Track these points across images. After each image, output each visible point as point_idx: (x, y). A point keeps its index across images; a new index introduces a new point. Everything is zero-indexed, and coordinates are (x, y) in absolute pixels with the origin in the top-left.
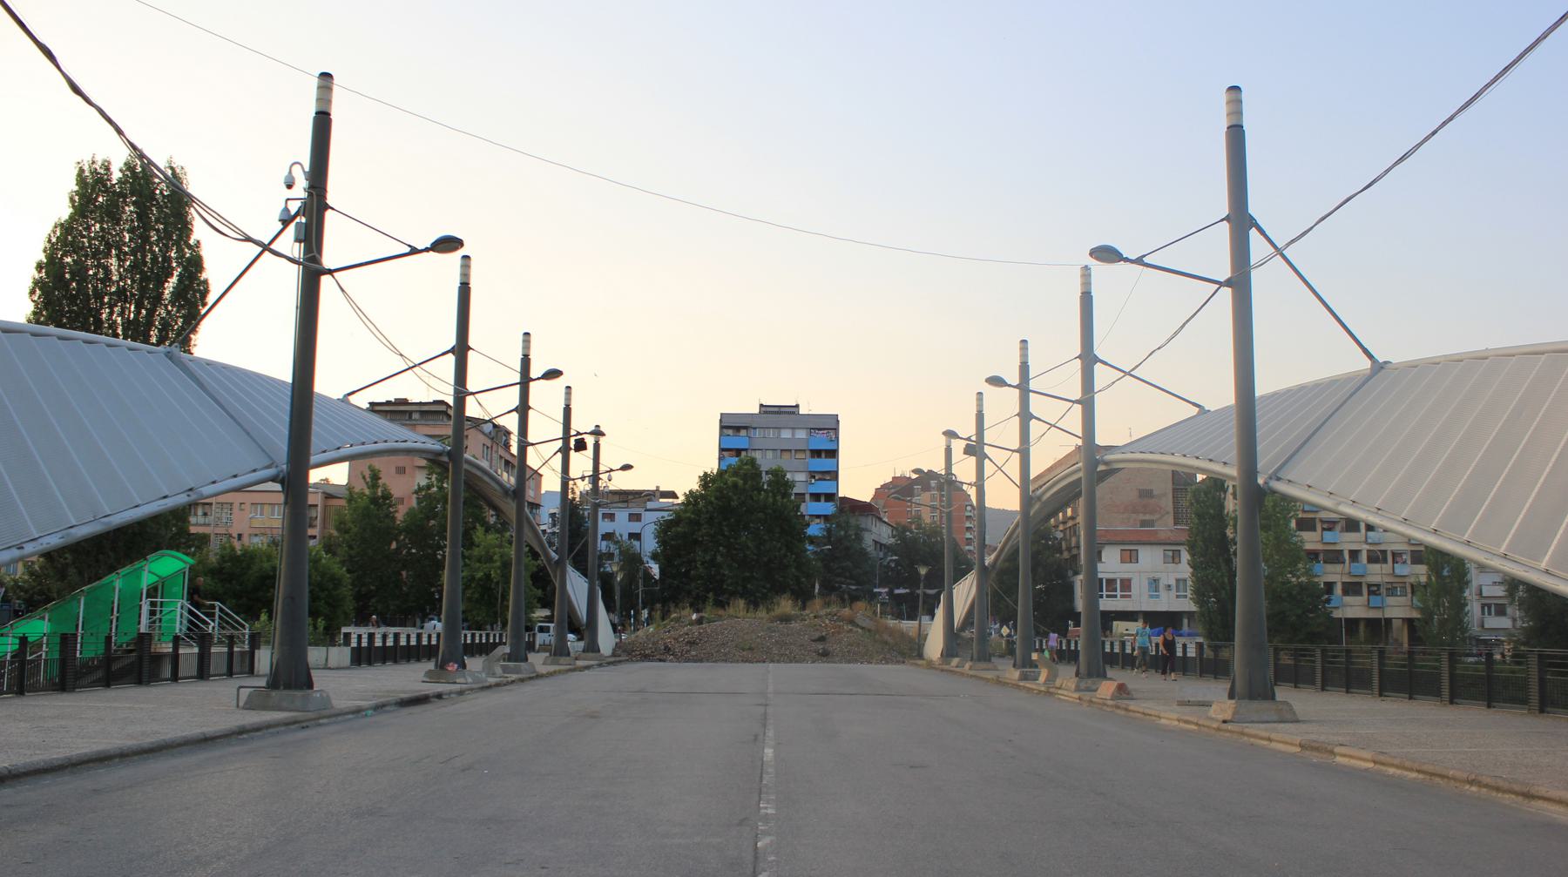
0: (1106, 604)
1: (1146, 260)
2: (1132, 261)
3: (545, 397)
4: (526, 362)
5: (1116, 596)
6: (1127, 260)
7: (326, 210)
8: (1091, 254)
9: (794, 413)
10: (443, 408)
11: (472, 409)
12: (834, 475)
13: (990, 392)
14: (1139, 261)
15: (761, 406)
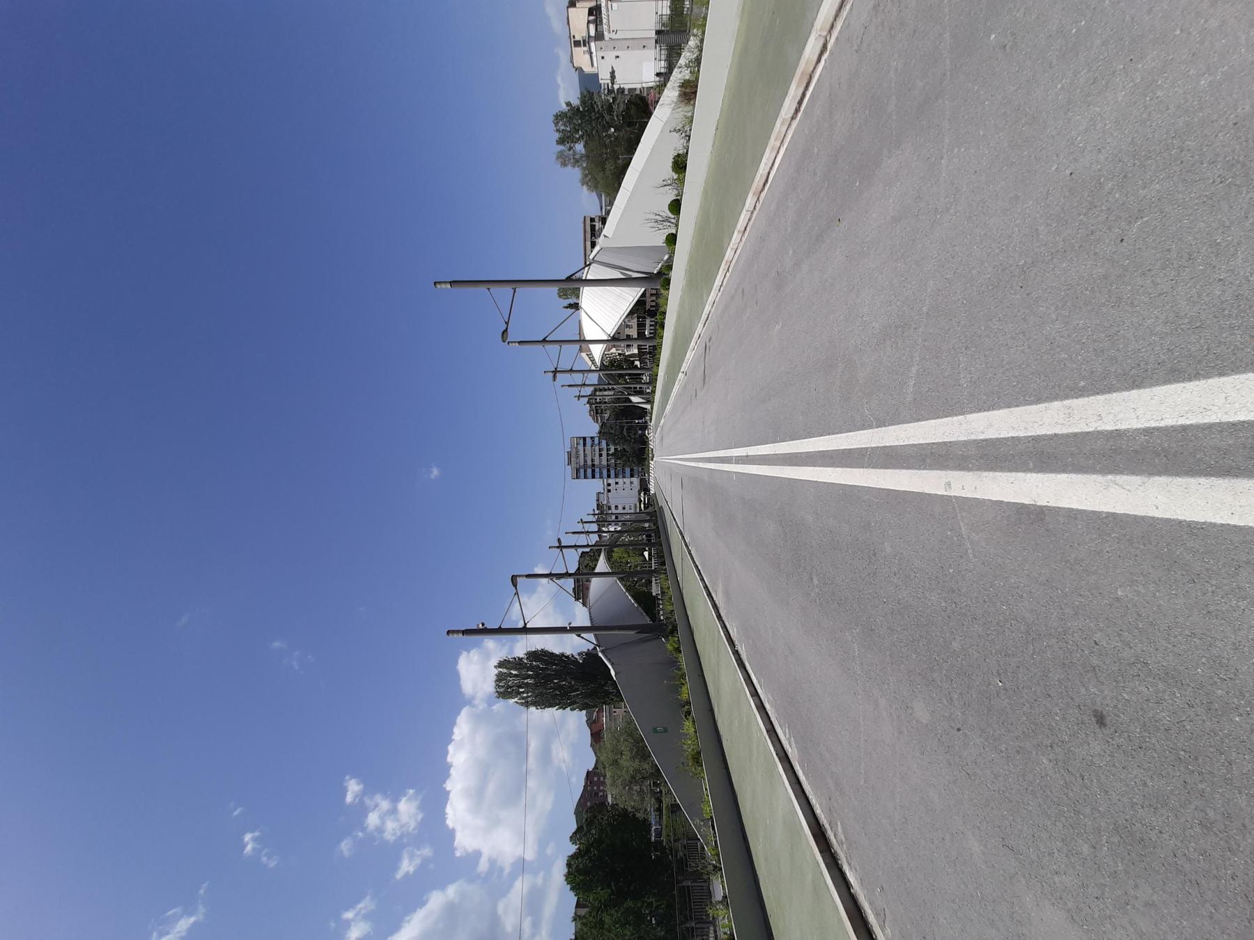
1: (507, 321)
4: (558, 547)
6: (507, 328)
14: (507, 323)
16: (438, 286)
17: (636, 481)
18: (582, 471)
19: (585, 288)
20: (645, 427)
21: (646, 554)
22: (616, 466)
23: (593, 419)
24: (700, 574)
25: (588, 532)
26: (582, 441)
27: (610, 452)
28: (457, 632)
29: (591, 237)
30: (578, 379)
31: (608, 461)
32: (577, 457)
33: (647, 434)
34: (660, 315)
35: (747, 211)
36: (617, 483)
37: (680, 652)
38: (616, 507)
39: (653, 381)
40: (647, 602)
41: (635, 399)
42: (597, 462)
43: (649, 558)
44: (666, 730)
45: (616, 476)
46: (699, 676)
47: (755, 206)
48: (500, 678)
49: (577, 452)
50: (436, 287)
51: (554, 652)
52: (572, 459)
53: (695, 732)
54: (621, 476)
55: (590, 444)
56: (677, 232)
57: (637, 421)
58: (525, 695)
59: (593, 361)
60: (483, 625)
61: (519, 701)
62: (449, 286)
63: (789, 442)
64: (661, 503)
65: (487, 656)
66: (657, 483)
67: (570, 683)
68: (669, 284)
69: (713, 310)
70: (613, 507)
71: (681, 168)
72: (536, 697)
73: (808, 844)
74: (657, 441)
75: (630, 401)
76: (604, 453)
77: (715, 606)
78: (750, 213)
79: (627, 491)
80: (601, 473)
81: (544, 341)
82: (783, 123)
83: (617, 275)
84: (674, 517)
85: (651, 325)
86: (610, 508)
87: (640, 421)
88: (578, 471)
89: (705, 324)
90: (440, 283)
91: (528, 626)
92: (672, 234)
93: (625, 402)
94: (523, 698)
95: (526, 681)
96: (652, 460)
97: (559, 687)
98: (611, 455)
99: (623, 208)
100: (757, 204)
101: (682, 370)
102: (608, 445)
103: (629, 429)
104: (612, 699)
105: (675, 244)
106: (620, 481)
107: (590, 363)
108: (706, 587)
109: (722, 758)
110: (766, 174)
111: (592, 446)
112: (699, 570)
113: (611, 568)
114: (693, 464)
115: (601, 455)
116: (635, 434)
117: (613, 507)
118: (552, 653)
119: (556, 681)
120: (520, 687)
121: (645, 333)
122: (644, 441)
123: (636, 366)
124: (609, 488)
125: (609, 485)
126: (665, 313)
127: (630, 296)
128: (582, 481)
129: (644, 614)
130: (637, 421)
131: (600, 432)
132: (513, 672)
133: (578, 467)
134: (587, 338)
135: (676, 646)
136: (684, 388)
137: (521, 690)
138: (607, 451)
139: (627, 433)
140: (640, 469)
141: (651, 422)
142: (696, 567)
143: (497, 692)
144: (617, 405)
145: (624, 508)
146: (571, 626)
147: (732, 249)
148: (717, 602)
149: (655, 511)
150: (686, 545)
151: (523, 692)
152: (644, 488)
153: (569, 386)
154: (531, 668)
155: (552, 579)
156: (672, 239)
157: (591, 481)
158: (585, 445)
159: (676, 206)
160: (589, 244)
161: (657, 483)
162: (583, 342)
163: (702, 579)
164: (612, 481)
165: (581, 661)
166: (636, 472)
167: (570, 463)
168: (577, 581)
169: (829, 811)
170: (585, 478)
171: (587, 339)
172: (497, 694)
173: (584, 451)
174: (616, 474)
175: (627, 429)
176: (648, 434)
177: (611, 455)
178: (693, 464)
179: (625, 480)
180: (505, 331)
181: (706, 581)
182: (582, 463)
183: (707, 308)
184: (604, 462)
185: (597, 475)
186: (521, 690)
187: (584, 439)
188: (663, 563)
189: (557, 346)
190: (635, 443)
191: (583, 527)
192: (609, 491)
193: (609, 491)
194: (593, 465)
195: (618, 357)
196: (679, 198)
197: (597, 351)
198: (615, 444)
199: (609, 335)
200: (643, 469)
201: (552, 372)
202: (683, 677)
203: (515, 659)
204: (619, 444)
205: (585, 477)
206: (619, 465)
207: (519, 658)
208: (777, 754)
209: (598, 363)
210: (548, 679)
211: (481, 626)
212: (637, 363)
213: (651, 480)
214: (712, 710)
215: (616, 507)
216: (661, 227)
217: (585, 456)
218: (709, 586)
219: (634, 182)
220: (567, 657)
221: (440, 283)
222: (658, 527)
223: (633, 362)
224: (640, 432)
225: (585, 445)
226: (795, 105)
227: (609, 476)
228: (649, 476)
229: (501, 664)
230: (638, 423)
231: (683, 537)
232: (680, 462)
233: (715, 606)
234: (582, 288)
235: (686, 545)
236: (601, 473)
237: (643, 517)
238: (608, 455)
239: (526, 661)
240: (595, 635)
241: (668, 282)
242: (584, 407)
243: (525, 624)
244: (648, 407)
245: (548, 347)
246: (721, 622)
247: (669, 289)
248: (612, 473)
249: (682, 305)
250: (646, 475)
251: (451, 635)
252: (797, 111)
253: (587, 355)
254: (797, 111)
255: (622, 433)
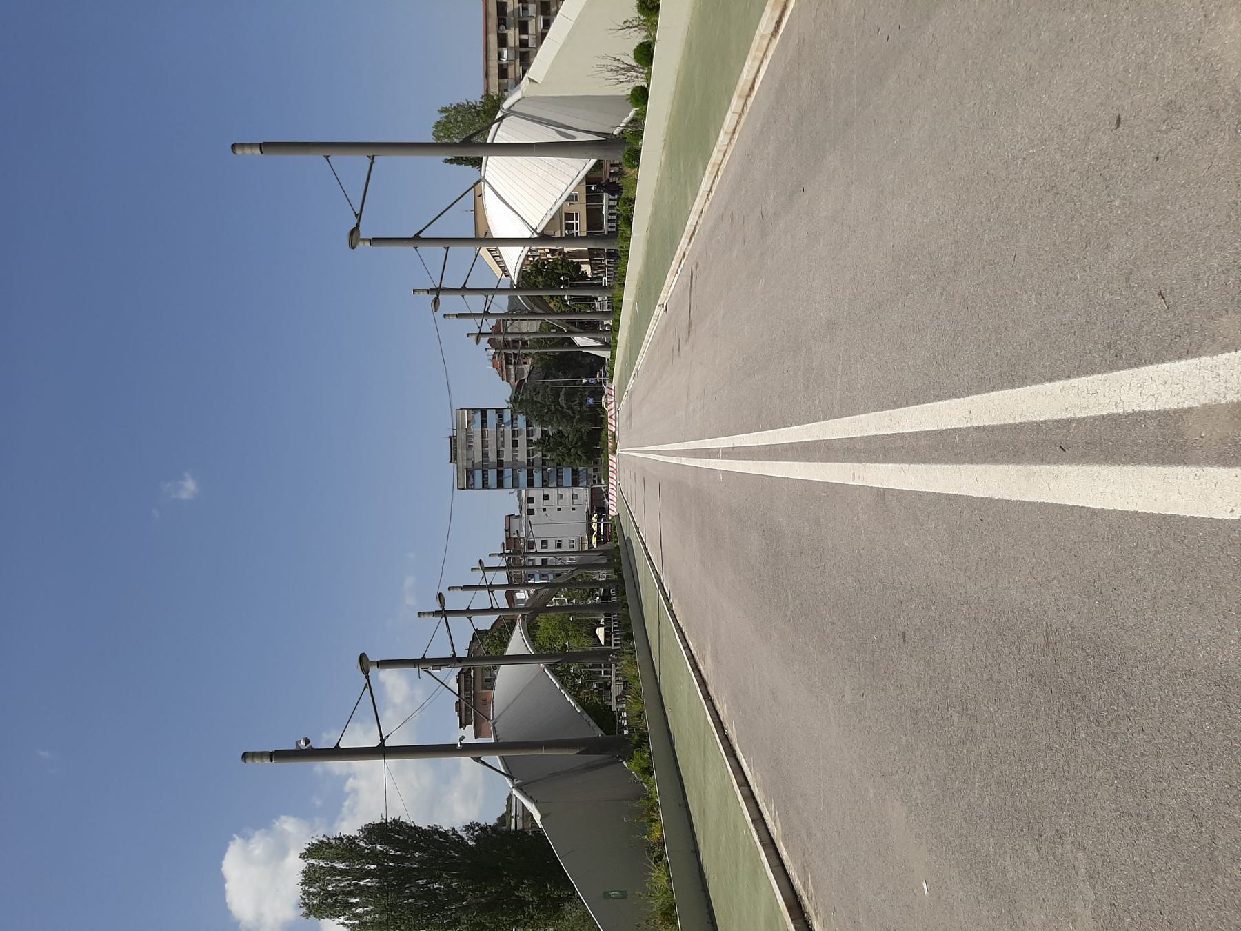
0: (582, 230)
1: (358, 212)
2: (359, 221)
3: (456, 601)
4: (436, 613)
5: (577, 224)
6: (358, 225)
7: (339, 747)
8: (353, 248)
9: (456, 440)
10: (462, 676)
11: (462, 652)
12: (499, 411)
13: (443, 308)
14: (359, 216)
15: (451, 462)
16: (239, 152)
17: (582, 493)
18: (478, 473)
19: (490, 157)
20: (598, 392)
21: (600, 632)
22: (544, 464)
23: (501, 374)
24: (683, 639)
25: (491, 586)
26: (478, 417)
27: (534, 439)
28: (261, 755)
29: (499, 25)
30: (476, 303)
31: (528, 455)
32: (469, 447)
33: (603, 404)
34: (625, 203)
35: (733, 113)
36: (546, 497)
37: (651, 774)
38: (544, 543)
39: (615, 308)
40: (604, 717)
41: (582, 341)
42: (507, 458)
43: (606, 642)
44: (624, 895)
45: (545, 484)
46: (692, 851)
47: (743, 109)
48: (310, 877)
49: (469, 437)
50: (234, 153)
51: (418, 825)
52: (459, 451)
53: (669, 881)
54: (555, 484)
55: (495, 422)
56: (648, 86)
57: (585, 381)
58: (360, 910)
59: (504, 269)
60: (307, 742)
61: (346, 922)
62: (258, 151)
63: (770, 431)
64: (628, 531)
65: (281, 852)
66: (621, 495)
67: (448, 885)
68: (637, 158)
69: (700, 223)
70: (538, 543)
71: (650, 9)
72: (381, 913)
73: (784, 921)
74: (623, 417)
75: (573, 344)
76: (522, 439)
77: (703, 683)
78: (737, 115)
79: (566, 513)
80: (515, 479)
81: (417, 238)
82: (762, 37)
83: (550, 136)
84: (648, 555)
85: (609, 221)
86: (531, 544)
87: (592, 380)
88: (470, 473)
89: (691, 239)
90: (243, 145)
91: (386, 744)
92: (642, 87)
93: (562, 346)
94: (356, 916)
95: (362, 883)
96: (614, 452)
97: (430, 894)
98: (535, 444)
99: (561, 43)
100: (745, 108)
101: (659, 303)
102: (528, 424)
103: (570, 395)
104: (531, 917)
105: (646, 103)
106: (552, 492)
107: (499, 272)
108: (691, 658)
109: (709, 920)
110: (751, 81)
111: (498, 426)
112: (683, 634)
113: (535, 648)
114: (674, 460)
115: (515, 444)
116: (581, 404)
117: (538, 543)
118: (416, 828)
119: (420, 882)
120: (351, 894)
121: (601, 210)
122: (598, 417)
123: (584, 275)
124: (531, 506)
125: (530, 500)
126: (632, 201)
127: (573, 170)
128: (478, 494)
129: (593, 724)
130: (585, 381)
131: (514, 400)
132: (340, 866)
133: (470, 466)
134: (497, 233)
135: (645, 765)
136: (664, 331)
137: (353, 901)
138: (528, 435)
139: (567, 401)
140: (591, 471)
141: (611, 382)
142: (679, 629)
143: (305, 904)
144: (547, 351)
145: (559, 546)
146: (463, 742)
147: (719, 151)
148: (705, 676)
149: (618, 547)
150: (666, 599)
151: (356, 905)
152: (598, 506)
153: (460, 315)
154: (373, 856)
155: (426, 670)
156: (641, 96)
157: (494, 494)
158: (484, 423)
159: (645, 53)
160: (493, 39)
161: (621, 495)
162: (484, 239)
163: (687, 647)
164: (536, 493)
165: (471, 843)
166: (582, 475)
167: (454, 458)
168: (463, 678)
169: (803, 873)
170: (484, 487)
171: (494, 237)
172: (304, 909)
173: (483, 436)
174: (543, 481)
175: (566, 395)
176: (606, 403)
177: (535, 444)
178: (674, 460)
179: (562, 491)
180: (355, 231)
181: (692, 648)
182: (478, 459)
183: (692, 219)
184: (522, 457)
185: (508, 481)
186: (353, 901)
187: (484, 412)
188: (629, 637)
189: (440, 250)
190: (580, 421)
191: (484, 576)
192: (531, 512)
193: (531, 512)
194: (500, 463)
195: (549, 256)
196: (650, 39)
197: (513, 257)
198: (542, 422)
199: (535, 230)
200: (595, 470)
201: (430, 291)
202: (653, 808)
203: (341, 839)
204: (549, 422)
205: (485, 486)
206: (550, 463)
207: (348, 837)
208: (760, 842)
209: (514, 273)
210: (406, 876)
211: (303, 743)
212: (586, 268)
213: (610, 491)
214: (696, 851)
215: (544, 543)
216: (622, 78)
217: (484, 444)
218: (695, 656)
219: (579, 9)
220: (444, 835)
221: (243, 145)
222: (621, 576)
223: (578, 266)
224: (591, 401)
225: (484, 423)
226: (773, 25)
227: (530, 484)
228: (607, 483)
229: (313, 852)
230: (588, 383)
231: (661, 586)
232: (656, 457)
233: (703, 683)
234: (484, 158)
235: (666, 599)
236: (515, 479)
237: (595, 558)
238: (529, 443)
239: (362, 844)
240: (503, 759)
241: (635, 155)
242: (483, 353)
243: (383, 740)
244: (606, 354)
245: (424, 249)
246: (709, 703)
247: (638, 165)
248: (537, 477)
249: (660, 191)
250: (603, 482)
251: (249, 762)
252: (776, 31)
253: (490, 251)
254: (776, 31)
255: (556, 402)
